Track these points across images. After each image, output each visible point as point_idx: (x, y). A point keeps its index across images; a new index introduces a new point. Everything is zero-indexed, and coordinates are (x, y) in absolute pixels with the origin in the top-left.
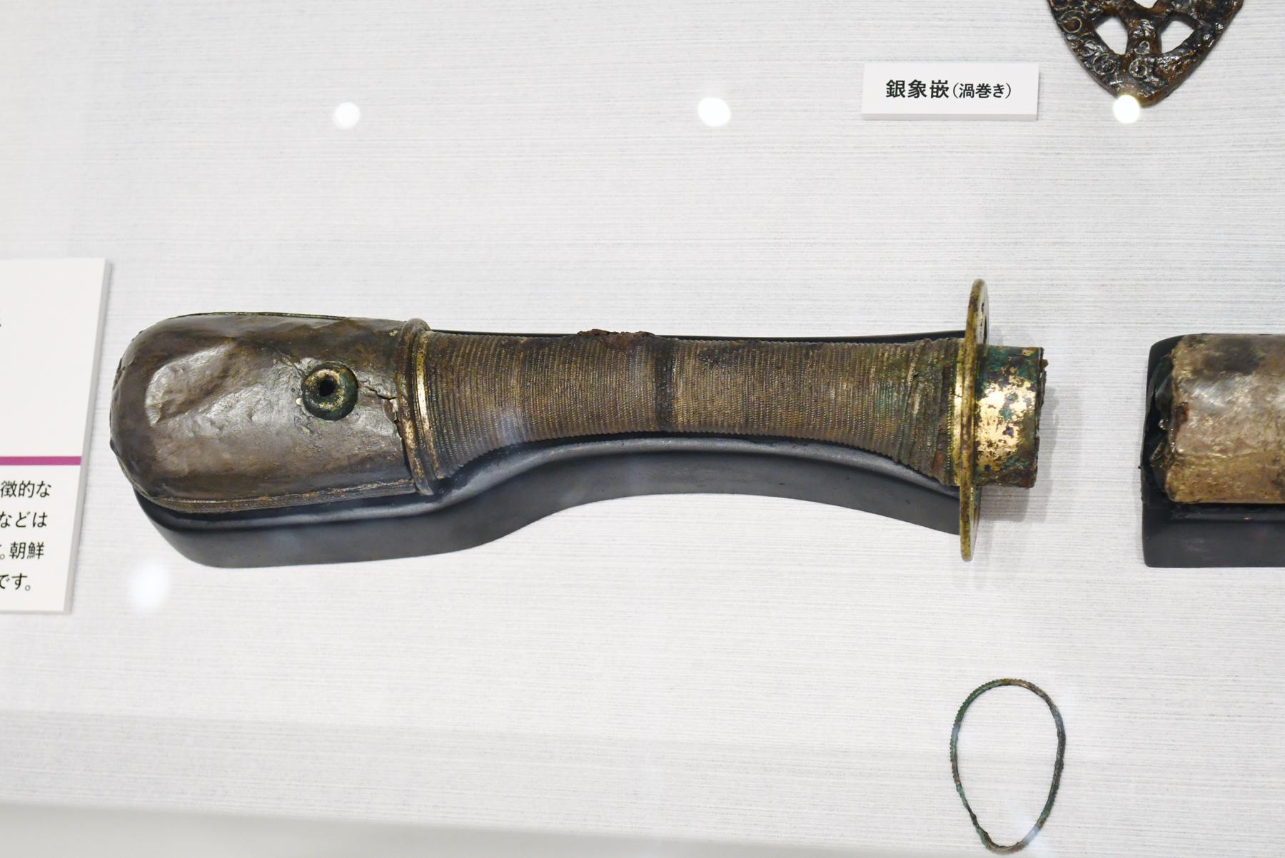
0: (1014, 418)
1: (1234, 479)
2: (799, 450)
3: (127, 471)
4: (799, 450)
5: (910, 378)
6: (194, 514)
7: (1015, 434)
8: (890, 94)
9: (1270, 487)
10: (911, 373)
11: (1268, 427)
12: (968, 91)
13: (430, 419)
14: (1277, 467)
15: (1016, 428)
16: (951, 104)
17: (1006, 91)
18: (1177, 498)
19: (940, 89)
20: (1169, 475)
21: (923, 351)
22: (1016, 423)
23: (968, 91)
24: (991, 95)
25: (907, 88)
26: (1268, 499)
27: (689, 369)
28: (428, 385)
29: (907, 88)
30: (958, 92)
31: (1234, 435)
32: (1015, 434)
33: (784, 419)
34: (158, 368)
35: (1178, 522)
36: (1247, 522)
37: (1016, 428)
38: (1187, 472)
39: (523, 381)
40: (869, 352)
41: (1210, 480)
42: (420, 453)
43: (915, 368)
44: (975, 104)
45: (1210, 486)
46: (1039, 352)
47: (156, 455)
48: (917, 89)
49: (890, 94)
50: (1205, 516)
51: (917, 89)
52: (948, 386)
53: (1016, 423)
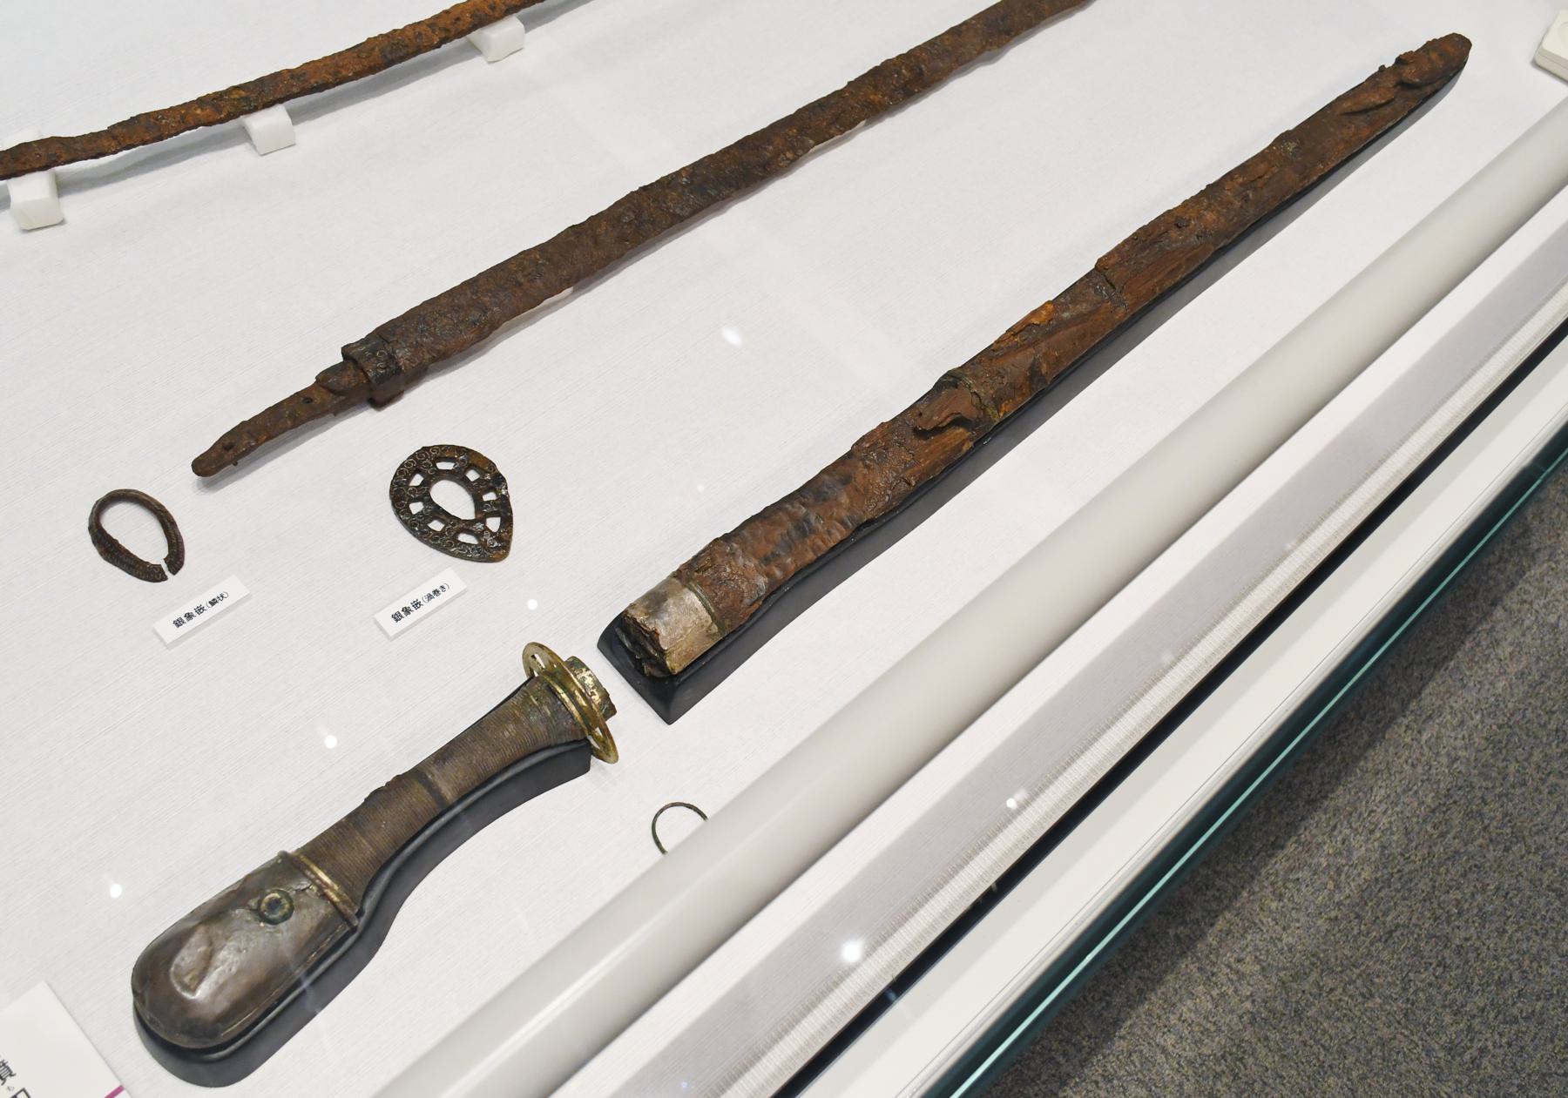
0: (591, 686)
1: (692, 646)
2: (232, 1048)
3: (227, 891)
4: (232, 1048)
5: (536, 703)
6: (333, 946)
7: (596, 693)
8: (397, 621)
9: (707, 640)
10: (534, 700)
11: (690, 614)
12: (430, 597)
13: (336, 883)
14: (704, 629)
15: (594, 691)
16: (427, 607)
17: (446, 586)
18: (676, 672)
19: (417, 605)
20: (668, 663)
21: (527, 698)
22: (593, 688)
23: (430, 597)
24: (441, 592)
25: (402, 613)
26: (709, 646)
27: (436, 772)
28: (322, 868)
29: (402, 613)
30: (426, 600)
31: (681, 626)
32: (596, 693)
33: (494, 762)
34: (183, 1048)
35: (679, 685)
36: (705, 665)
37: (594, 691)
38: (674, 656)
39: (363, 834)
40: (507, 708)
41: (684, 654)
42: (344, 902)
43: (534, 697)
44: (437, 601)
45: (685, 656)
46: (574, 658)
47: (230, 911)
48: (407, 611)
49: (397, 621)
50: (693, 671)
51: (407, 611)
52: (555, 694)
53: (593, 688)
